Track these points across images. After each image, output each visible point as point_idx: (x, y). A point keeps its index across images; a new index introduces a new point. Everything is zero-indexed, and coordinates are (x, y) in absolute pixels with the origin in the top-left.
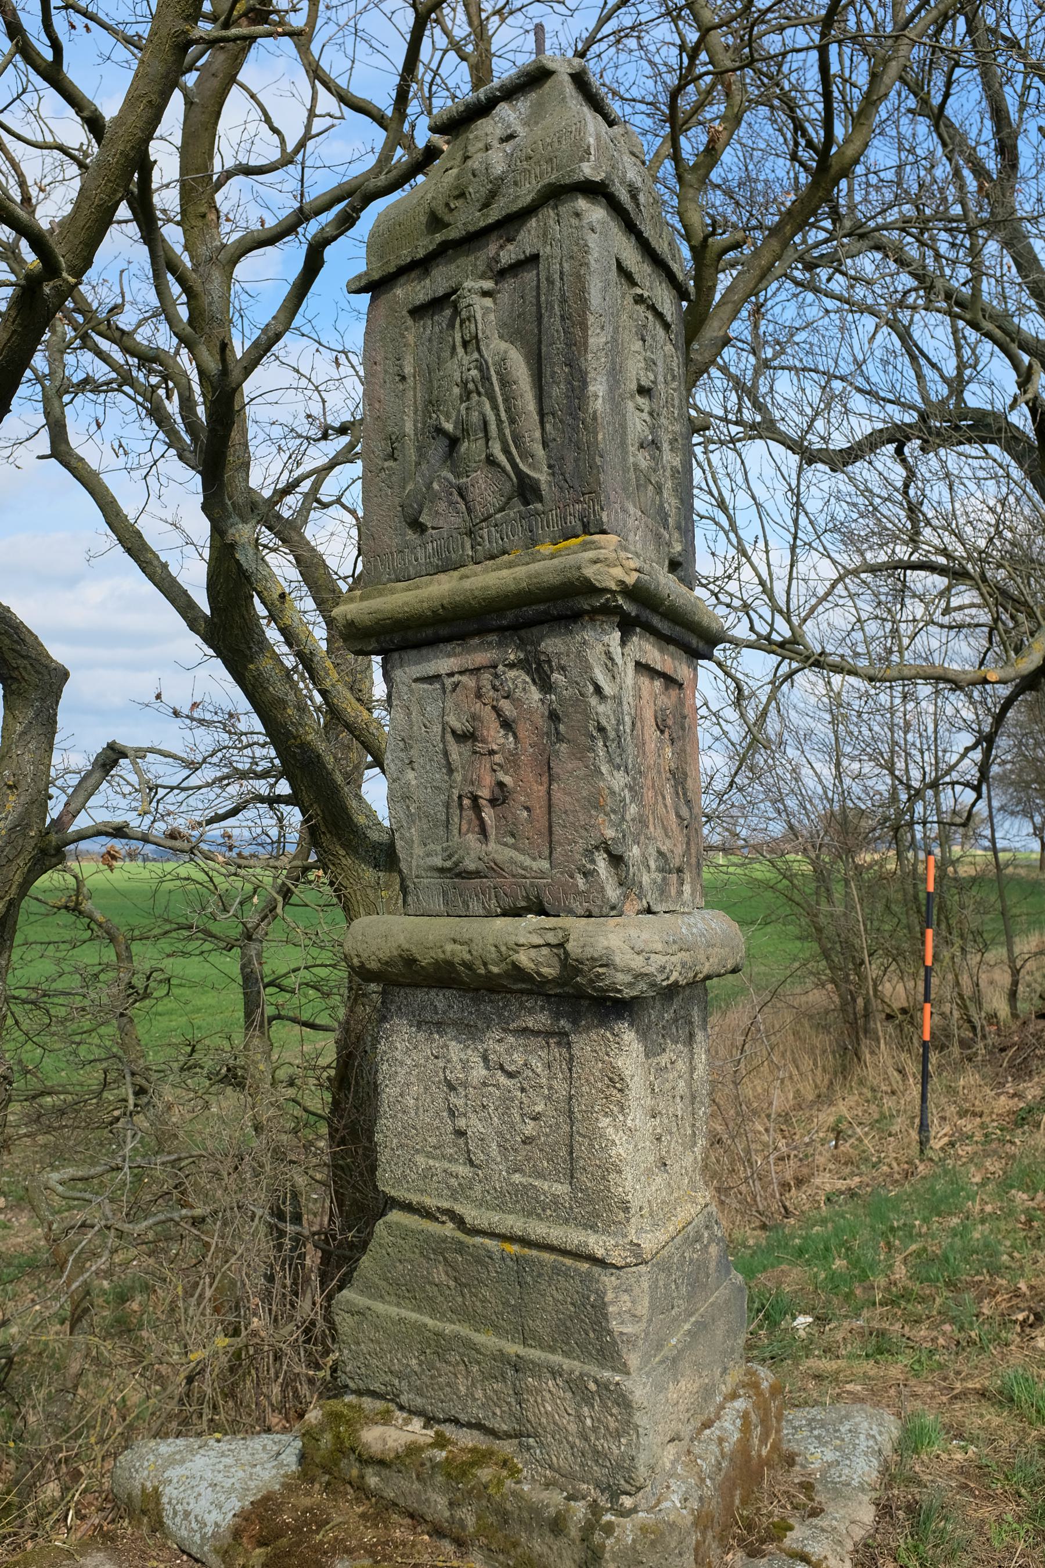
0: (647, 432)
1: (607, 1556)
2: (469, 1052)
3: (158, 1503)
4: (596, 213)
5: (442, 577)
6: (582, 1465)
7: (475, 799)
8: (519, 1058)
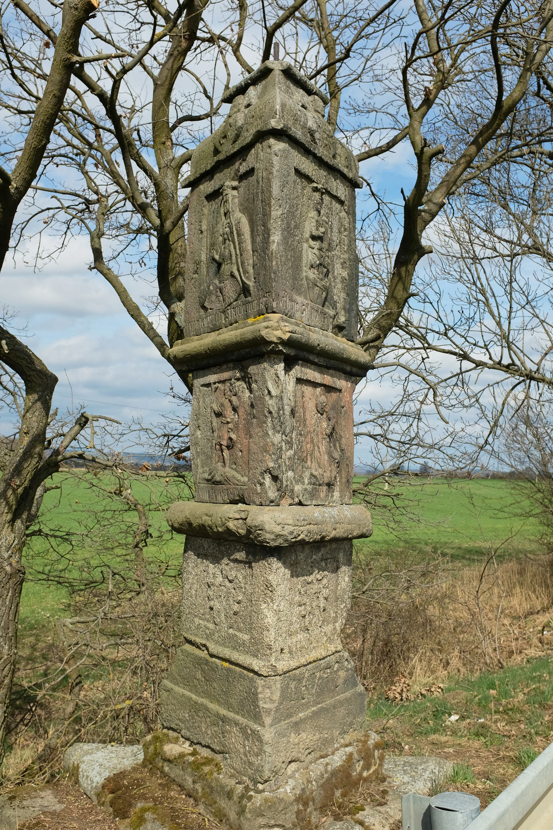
0: (316, 259)
1: (247, 810)
2: (216, 569)
3: (78, 771)
4: (278, 146)
5: (213, 333)
6: (244, 768)
7: (221, 445)
8: (233, 573)
